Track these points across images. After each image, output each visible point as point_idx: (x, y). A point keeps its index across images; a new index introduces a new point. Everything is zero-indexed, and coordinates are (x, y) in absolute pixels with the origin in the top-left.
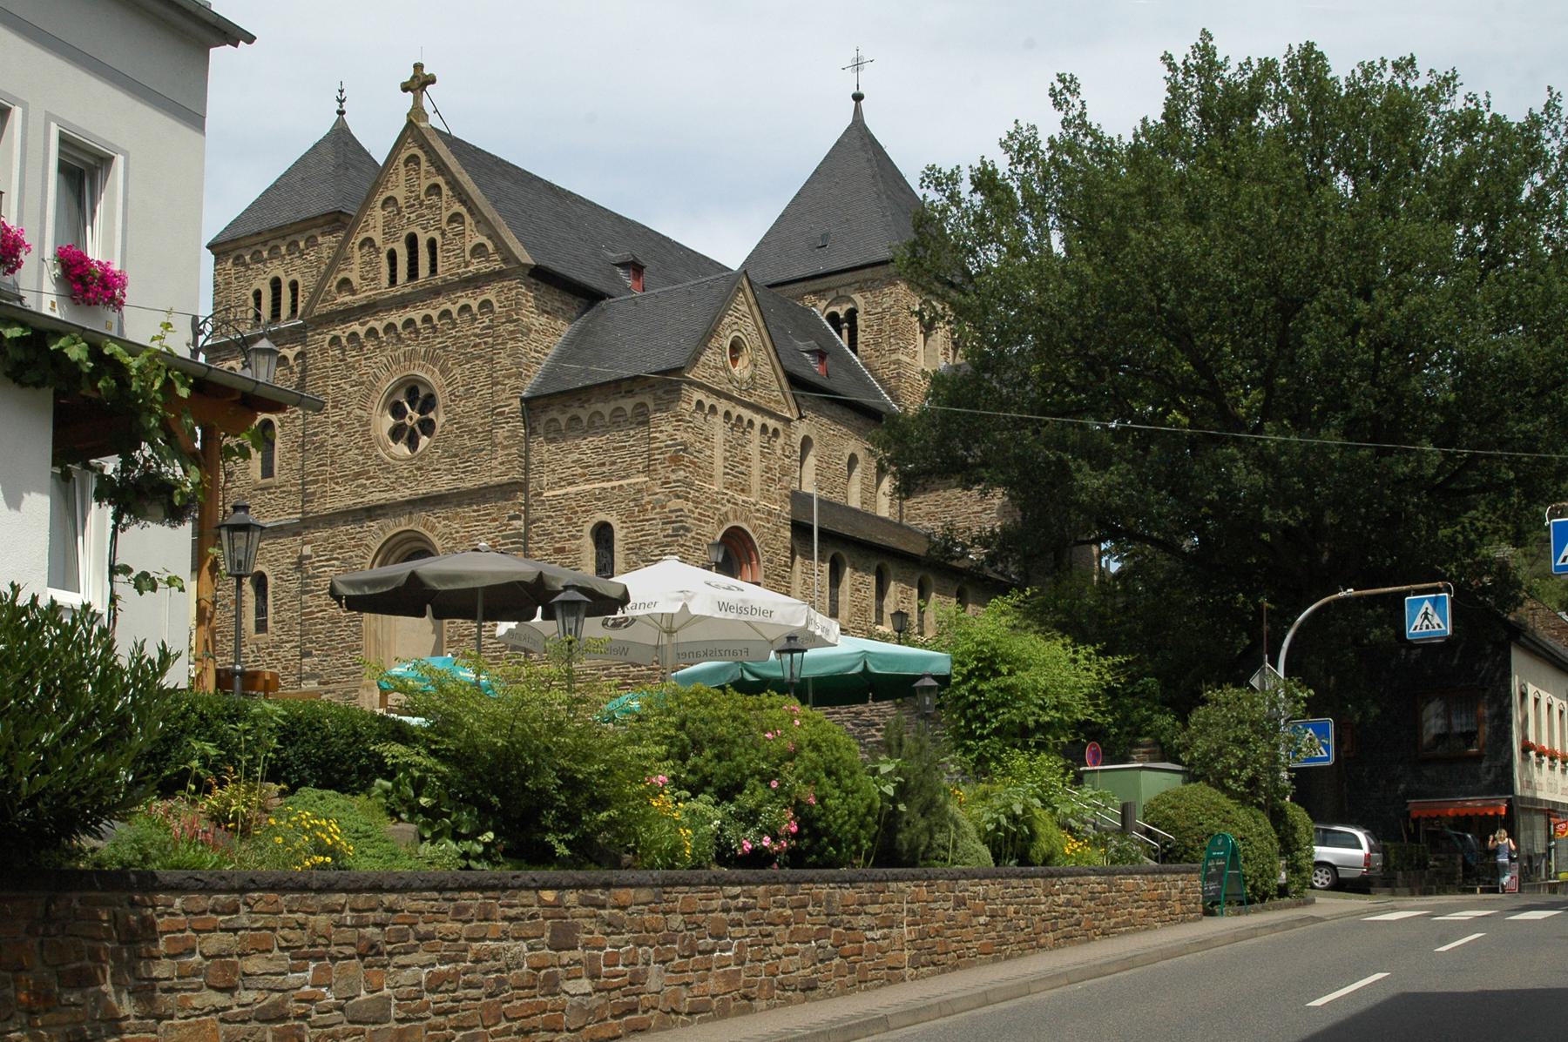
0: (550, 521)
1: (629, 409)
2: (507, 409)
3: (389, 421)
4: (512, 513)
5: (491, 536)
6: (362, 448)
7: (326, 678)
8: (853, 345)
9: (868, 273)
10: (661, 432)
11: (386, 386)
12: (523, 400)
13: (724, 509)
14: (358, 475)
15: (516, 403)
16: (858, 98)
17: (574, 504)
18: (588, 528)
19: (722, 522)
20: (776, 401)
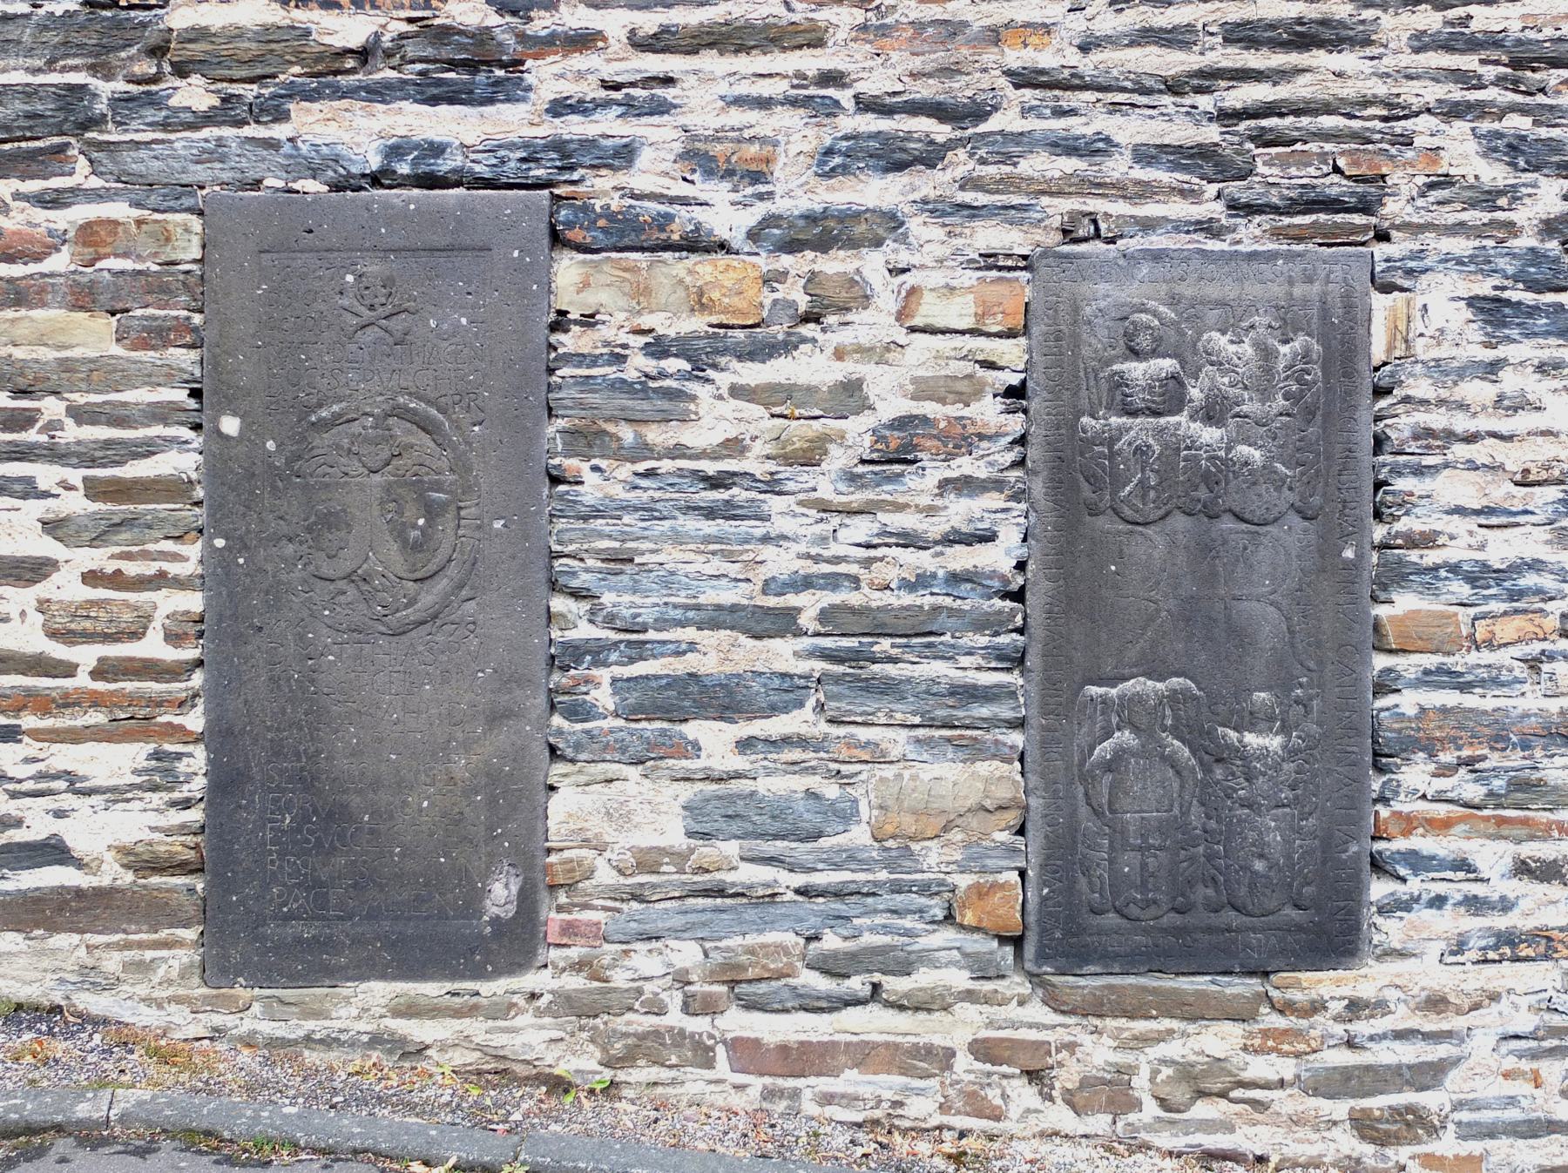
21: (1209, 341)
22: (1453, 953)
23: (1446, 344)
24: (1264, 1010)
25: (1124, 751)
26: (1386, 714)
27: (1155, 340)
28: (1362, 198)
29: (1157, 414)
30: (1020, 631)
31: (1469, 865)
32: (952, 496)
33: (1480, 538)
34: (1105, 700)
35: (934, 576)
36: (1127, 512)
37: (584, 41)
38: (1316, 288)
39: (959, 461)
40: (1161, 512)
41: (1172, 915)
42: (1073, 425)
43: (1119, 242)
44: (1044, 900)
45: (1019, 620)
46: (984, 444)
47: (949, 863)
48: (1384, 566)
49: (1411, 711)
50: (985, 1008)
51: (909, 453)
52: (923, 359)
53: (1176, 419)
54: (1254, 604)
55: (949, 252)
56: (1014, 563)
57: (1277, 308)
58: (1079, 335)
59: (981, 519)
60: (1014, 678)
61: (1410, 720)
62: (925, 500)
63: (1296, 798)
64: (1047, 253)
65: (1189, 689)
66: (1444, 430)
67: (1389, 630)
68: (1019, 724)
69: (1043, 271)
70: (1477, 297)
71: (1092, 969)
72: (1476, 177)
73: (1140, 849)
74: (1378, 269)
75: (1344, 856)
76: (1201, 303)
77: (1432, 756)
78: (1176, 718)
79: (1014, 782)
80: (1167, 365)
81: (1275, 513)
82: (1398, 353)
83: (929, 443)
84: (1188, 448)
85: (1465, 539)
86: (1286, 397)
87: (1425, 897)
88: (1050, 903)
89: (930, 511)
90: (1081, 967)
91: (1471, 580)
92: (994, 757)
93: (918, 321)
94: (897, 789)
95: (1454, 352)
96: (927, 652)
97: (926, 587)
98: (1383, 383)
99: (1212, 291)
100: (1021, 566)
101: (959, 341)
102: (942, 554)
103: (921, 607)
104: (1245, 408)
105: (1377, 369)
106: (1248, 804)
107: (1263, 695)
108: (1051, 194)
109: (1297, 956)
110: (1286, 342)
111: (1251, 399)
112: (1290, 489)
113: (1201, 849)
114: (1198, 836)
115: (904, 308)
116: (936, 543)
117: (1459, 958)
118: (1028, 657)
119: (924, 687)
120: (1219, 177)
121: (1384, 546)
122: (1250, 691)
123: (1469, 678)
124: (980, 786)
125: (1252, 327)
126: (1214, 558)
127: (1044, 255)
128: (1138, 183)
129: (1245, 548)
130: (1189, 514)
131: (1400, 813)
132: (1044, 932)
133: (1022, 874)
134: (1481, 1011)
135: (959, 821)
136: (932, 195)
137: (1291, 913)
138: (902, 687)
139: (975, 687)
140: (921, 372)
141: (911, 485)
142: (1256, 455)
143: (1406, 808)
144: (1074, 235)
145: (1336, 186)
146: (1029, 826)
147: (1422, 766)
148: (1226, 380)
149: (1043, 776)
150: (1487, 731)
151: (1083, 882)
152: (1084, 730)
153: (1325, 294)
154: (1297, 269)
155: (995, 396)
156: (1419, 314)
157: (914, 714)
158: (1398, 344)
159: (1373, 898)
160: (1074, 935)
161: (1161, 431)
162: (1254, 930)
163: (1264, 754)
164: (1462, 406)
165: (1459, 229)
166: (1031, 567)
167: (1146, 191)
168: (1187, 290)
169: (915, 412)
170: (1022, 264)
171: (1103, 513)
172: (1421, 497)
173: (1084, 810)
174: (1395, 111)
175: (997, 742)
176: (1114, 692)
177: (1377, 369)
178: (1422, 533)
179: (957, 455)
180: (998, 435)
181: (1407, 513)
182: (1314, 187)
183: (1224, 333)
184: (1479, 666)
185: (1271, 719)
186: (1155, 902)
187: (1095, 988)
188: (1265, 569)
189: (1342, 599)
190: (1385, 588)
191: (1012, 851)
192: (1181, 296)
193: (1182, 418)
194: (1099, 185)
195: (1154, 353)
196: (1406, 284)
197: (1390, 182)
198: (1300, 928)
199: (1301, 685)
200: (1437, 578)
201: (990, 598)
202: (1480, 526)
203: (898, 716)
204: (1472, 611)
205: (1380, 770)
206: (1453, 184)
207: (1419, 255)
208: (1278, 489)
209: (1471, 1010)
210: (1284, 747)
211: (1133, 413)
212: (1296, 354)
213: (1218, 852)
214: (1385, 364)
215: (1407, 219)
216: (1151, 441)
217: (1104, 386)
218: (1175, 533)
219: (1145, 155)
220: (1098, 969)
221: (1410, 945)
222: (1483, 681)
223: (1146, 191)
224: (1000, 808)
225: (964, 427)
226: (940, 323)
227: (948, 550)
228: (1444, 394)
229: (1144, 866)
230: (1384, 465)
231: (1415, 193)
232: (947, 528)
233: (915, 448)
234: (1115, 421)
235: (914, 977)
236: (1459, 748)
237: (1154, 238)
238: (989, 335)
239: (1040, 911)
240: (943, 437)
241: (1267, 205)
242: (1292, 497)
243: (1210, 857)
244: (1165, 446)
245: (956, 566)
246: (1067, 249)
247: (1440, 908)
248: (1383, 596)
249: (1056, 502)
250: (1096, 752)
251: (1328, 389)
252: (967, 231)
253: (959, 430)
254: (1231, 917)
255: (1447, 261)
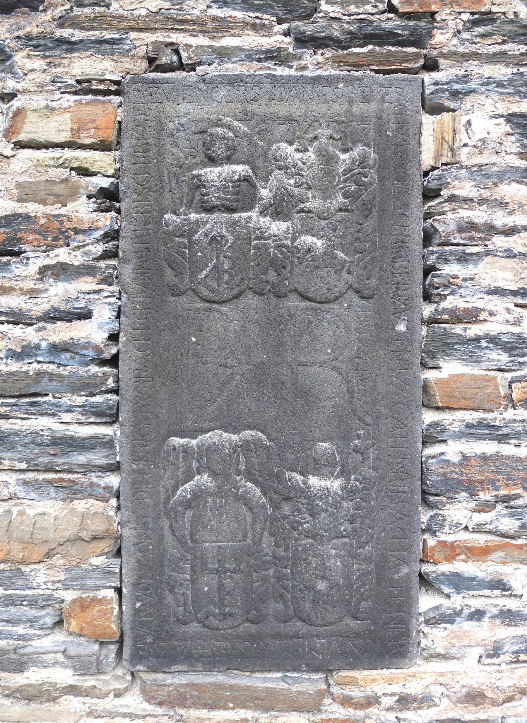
21: (277, 150)
22: (489, 656)
23: (487, 152)
24: (327, 701)
25: (202, 491)
26: (434, 460)
27: (229, 149)
28: (414, 31)
29: (231, 210)
30: (116, 391)
31: (505, 585)
32: (51, 281)
33: (516, 315)
34: (186, 449)
35: (38, 347)
36: (205, 292)
38: (373, 107)
39: (57, 251)
40: (235, 292)
41: (247, 625)
42: (159, 221)
43: (198, 68)
44: (137, 612)
45: (111, 383)
46: (80, 237)
47: (54, 582)
48: (432, 337)
49: (456, 459)
50: (87, 700)
51: (15, 245)
52: (25, 167)
53: (249, 214)
54: (318, 369)
55: (48, 78)
56: (106, 335)
57: (339, 123)
58: (163, 146)
59: (77, 299)
60: (107, 431)
61: (454, 465)
62: (29, 284)
63: (354, 530)
64: (136, 79)
65: (260, 440)
66: (485, 224)
67: (436, 390)
68: (116, 468)
69: (132, 94)
70: (514, 115)
71: (179, 667)
72: (515, 13)
73: (217, 572)
74: (427, 92)
75: (396, 577)
76: (271, 119)
77: (473, 495)
78: (249, 464)
79: (108, 517)
80: (241, 169)
81: (336, 292)
82: (444, 160)
83: (31, 237)
84: (258, 238)
85: (503, 316)
86: (345, 196)
87: (466, 611)
88: (141, 614)
89: (34, 294)
90: (169, 666)
91: (509, 349)
92: (90, 496)
93: (23, 137)
94: (7, 522)
95: (494, 159)
96: (33, 410)
97: (31, 356)
98: (431, 190)
99: (281, 110)
100: (114, 338)
101: (58, 153)
102: (44, 328)
103: (26, 373)
104: (308, 205)
105: (426, 174)
106: (314, 535)
107: (325, 445)
108: (140, 30)
109: (355, 657)
110: (346, 150)
111: (314, 197)
112: (349, 272)
113: (271, 572)
114: (269, 562)
115: (11, 126)
116: (39, 319)
117: (495, 660)
118: (120, 413)
119: (30, 439)
120: (288, 16)
121: (432, 321)
122: (314, 441)
123: (507, 431)
124: (77, 520)
125: (316, 138)
126: (282, 331)
127: (133, 81)
128: (215, 19)
129: (310, 322)
130: (260, 294)
131: (445, 542)
132: (136, 638)
133: (119, 591)
134: (514, 703)
135: (59, 549)
136: (35, 31)
137: (353, 623)
138: (11, 439)
139: (72, 438)
140: (24, 179)
141: (17, 272)
142: (319, 243)
143: (450, 539)
144: (158, 62)
146: (123, 552)
147: (464, 504)
148: (292, 181)
149: (134, 511)
150: (521, 475)
151: (169, 598)
152: (168, 474)
153: (381, 111)
154: (356, 91)
155: (89, 197)
156: (463, 129)
157: (20, 460)
158: (445, 152)
159: (421, 611)
160: (163, 640)
161: (234, 224)
162: (318, 637)
163: (325, 493)
164: (502, 204)
166: (122, 338)
168: (258, 108)
169: (19, 211)
170: (113, 88)
171: (184, 293)
172: (465, 280)
173: (169, 540)
175: (92, 484)
176: (194, 442)
177: (426, 174)
178: (466, 310)
179: (56, 247)
180: (91, 230)
181: (452, 293)
182: (371, 22)
183: (291, 144)
184: (515, 421)
185: (332, 465)
186: (231, 615)
187: (180, 686)
188: (327, 340)
189: (395, 365)
190: (433, 355)
191: (107, 573)
192: (254, 114)
193: (254, 214)
194: (182, 22)
195: (229, 160)
196: (453, 105)
197: (438, 19)
198: (357, 635)
199: (359, 437)
200: (479, 347)
201: (87, 365)
202: (516, 305)
203: (7, 462)
204: (509, 376)
205: (429, 506)
206: (494, 20)
207: (465, 78)
208: (338, 272)
209: (504, 702)
210: (343, 489)
211: (210, 210)
212: (354, 160)
213: (285, 575)
214: (434, 168)
215: (454, 49)
216: (225, 232)
217: (185, 188)
218: (248, 310)
220: (184, 668)
221: (453, 651)
222: (519, 433)
224: (94, 538)
225: (62, 223)
226: (41, 137)
227: (50, 326)
228: (485, 193)
229: (221, 586)
230: (432, 253)
231: (461, 27)
232: (47, 307)
233: (19, 241)
234: (193, 216)
235: (26, 674)
236: (497, 489)
237: (229, 66)
238: (84, 147)
239: (133, 621)
240: (43, 231)
241: (329, 38)
242: (350, 279)
243: (279, 578)
244: (237, 237)
245: (55, 338)
246: (153, 75)
247: (479, 620)
248: (431, 363)
249: (142, 285)
250: (179, 492)
251: (383, 190)
252: (65, 62)
253: (57, 225)
254: (297, 625)
255: (488, 83)
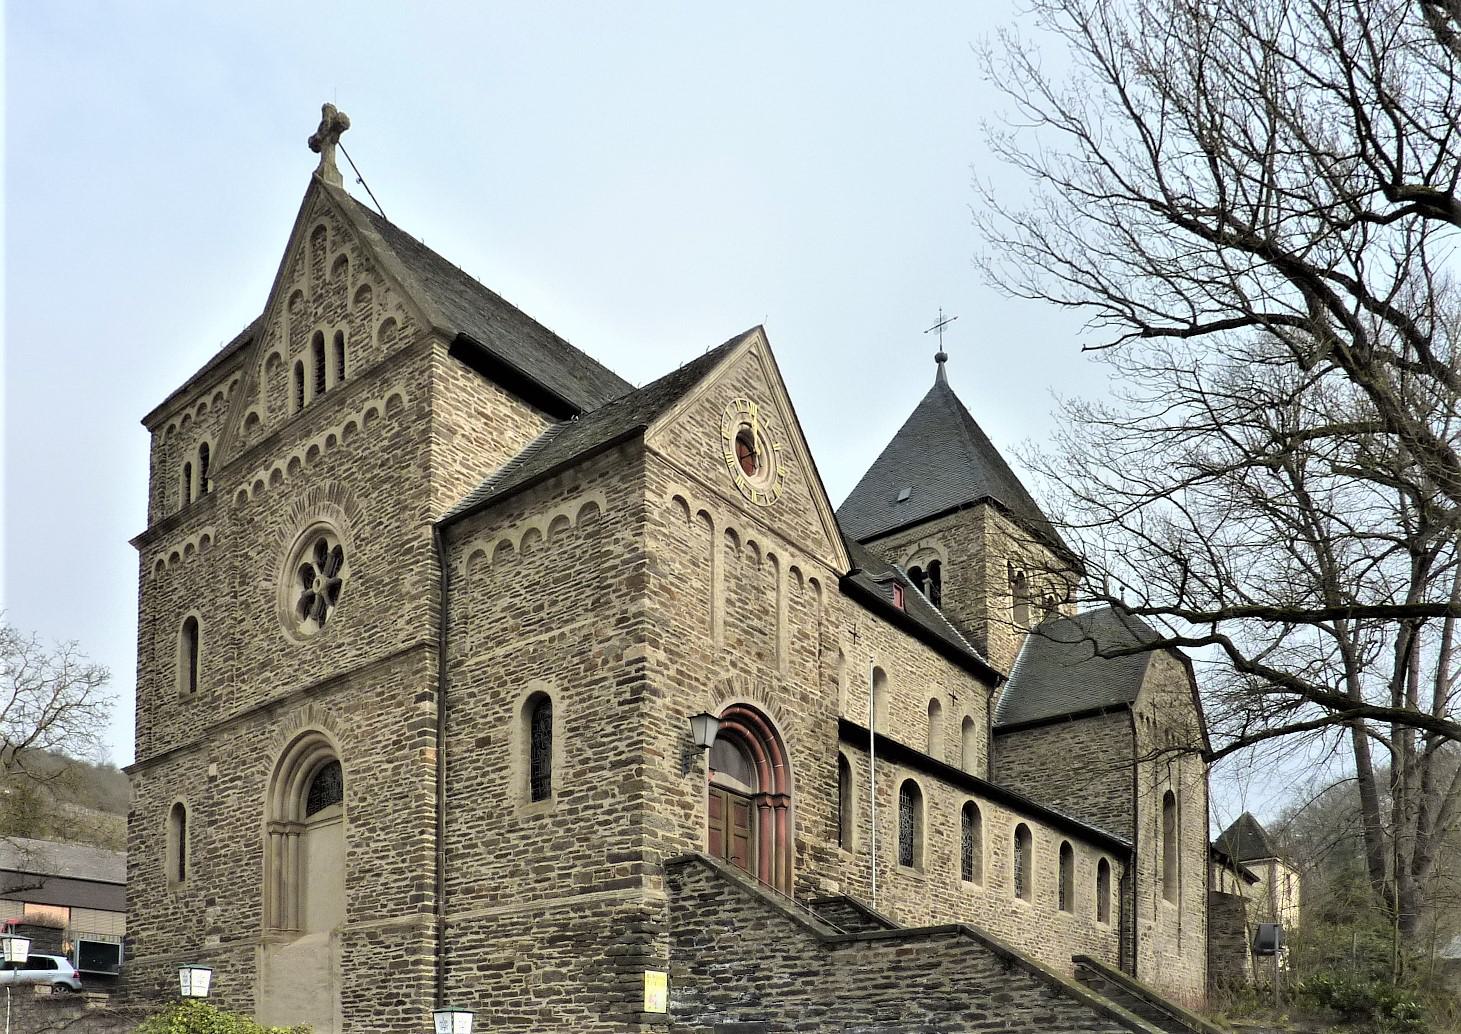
0: (472, 700)
1: (572, 516)
2: (415, 544)
3: (298, 592)
4: (419, 691)
5: (395, 727)
6: (267, 630)
7: (227, 934)
8: (936, 600)
9: (952, 520)
10: (617, 541)
11: (291, 544)
12: (435, 526)
13: (724, 675)
14: (263, 666)
15: (428, 532)
16: (941, 359)
17: (502, 671)
18: (518, 705)
19: (722, 696)
20: (814, 540)
37: (769, 995)
145: (892, 1015)
165: (914, 1022)
167: (858, 1018)
174: (903, 1000)
219: (859, 1011)
223: (858, 1018)
